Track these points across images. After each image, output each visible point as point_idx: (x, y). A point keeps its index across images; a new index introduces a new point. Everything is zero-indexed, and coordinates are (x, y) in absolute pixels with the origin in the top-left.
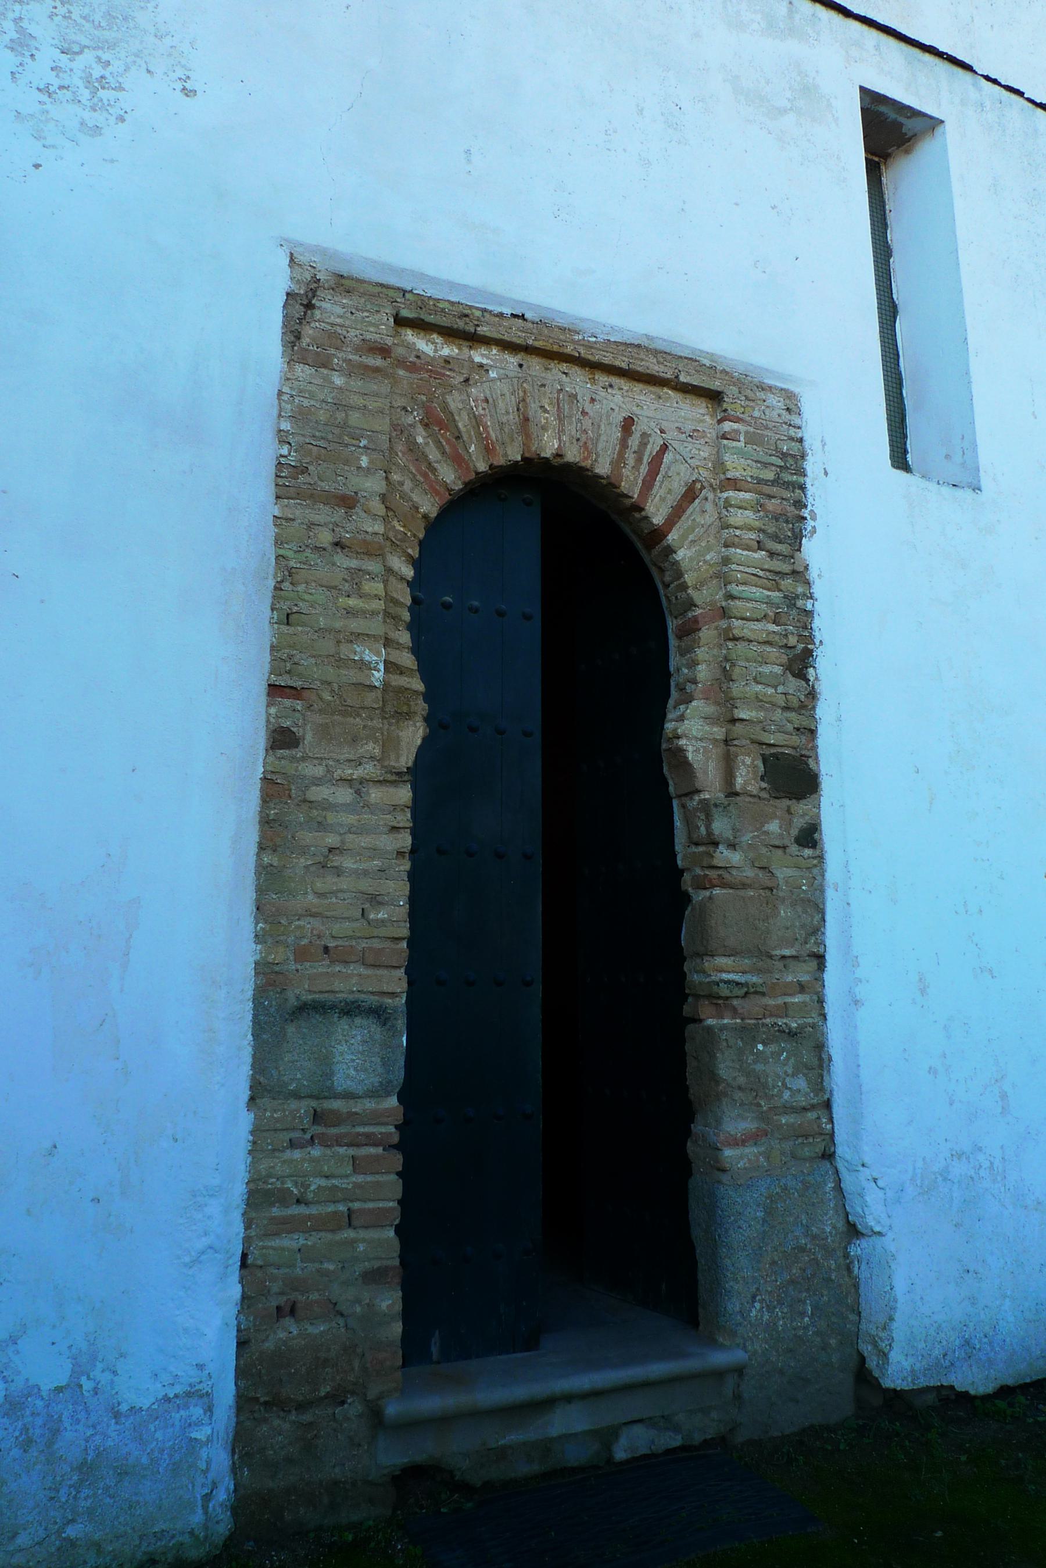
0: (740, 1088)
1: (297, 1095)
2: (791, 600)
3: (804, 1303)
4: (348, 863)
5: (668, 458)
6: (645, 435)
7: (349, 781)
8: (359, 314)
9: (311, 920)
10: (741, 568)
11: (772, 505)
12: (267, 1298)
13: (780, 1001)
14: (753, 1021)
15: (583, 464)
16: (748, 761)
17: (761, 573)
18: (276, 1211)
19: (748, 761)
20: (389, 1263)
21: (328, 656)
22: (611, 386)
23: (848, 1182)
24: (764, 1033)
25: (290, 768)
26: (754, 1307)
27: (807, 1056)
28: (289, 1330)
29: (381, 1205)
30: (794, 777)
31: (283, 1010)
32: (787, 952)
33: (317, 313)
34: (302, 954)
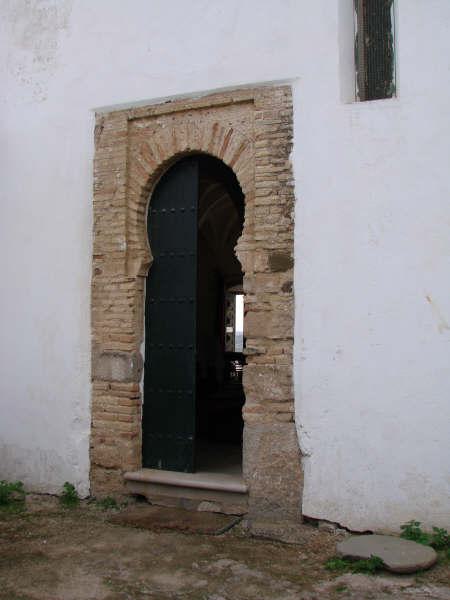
2: (283, 183)
11: (275, 143)
12: (98, 439)
23: (300, 433)
26: (255, 473)
27: (283, 379)
28: (102, 447)
30: (282, 262)
31: (101, 355)
32: (275, 337)
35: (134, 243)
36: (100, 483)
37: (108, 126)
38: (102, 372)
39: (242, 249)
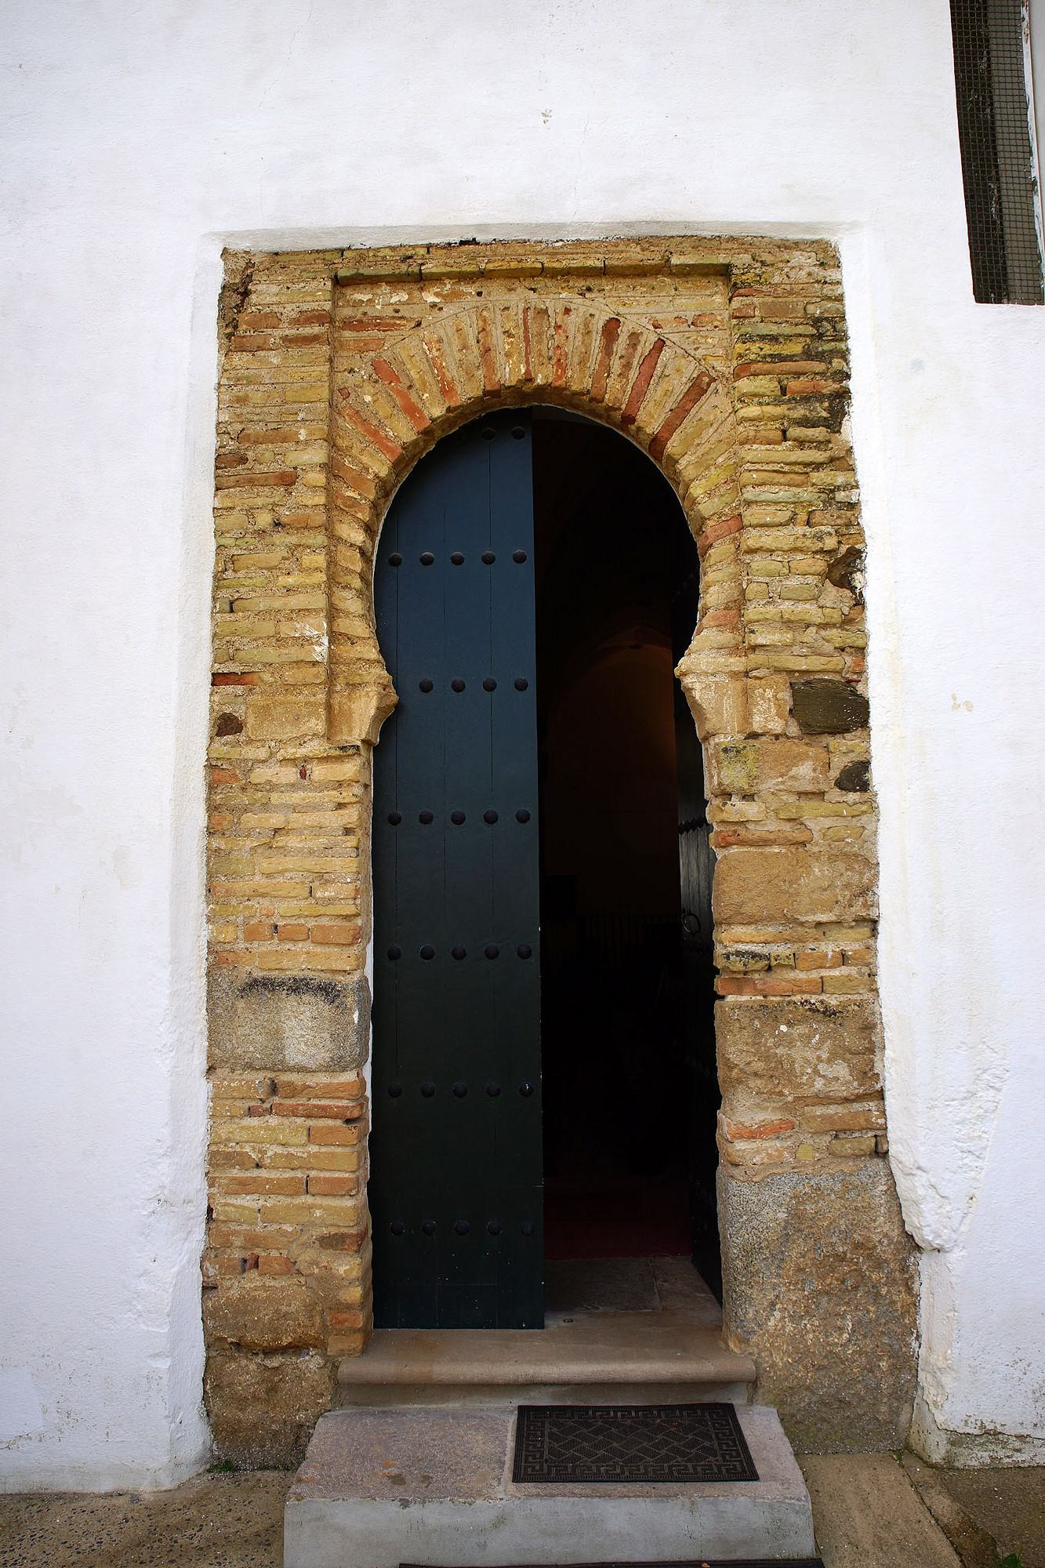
0: (756, 1074)
1: (250, 1066)
3: (843, 1317)
4: (293, 842)
5: (666, 354)
6: (634, 337)
7: (293, 761)
8: (294, 287)
9: (261, 900)
10: (758, 466)
12: (229, 1254)
13: (815, 975)
14: (778, 999)
15: (557, 384)
16: (769, 693)
17: (786, 468)
18: (236, 1172)
19: (769, 693)
20: (346, 1230)
21: (268, 638)
22: (589, 290)
24: (791, 1012)
25: (235, 754)
27: (850, 1038)
29: (337, 1175)
30: (834, 707)
31: (237, 988)
32: (823, 918)
33: (253, 298)
34: (251, 935)
35: (352, 640)
36: (242, 1402)
37: (265, 293)
38: (249, 1037)
39: (704, 667)
